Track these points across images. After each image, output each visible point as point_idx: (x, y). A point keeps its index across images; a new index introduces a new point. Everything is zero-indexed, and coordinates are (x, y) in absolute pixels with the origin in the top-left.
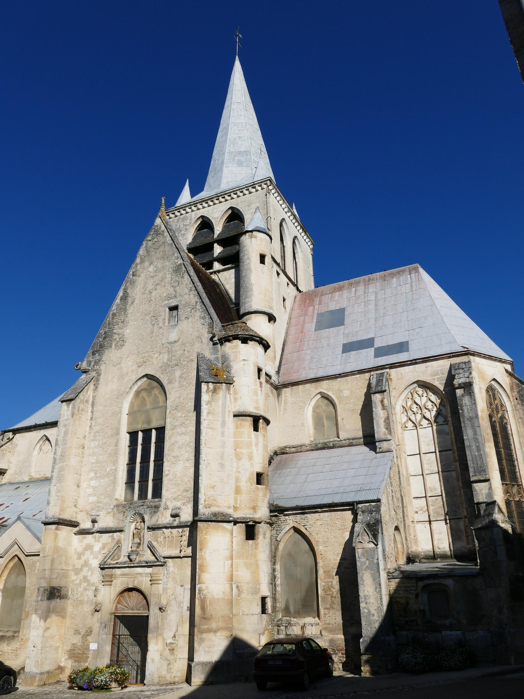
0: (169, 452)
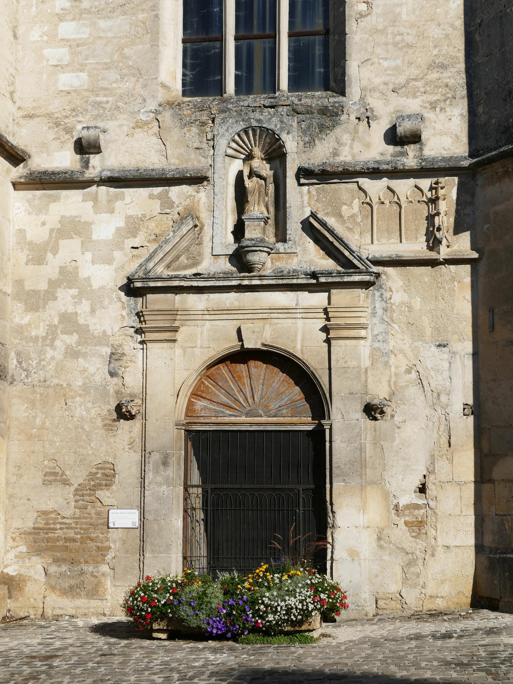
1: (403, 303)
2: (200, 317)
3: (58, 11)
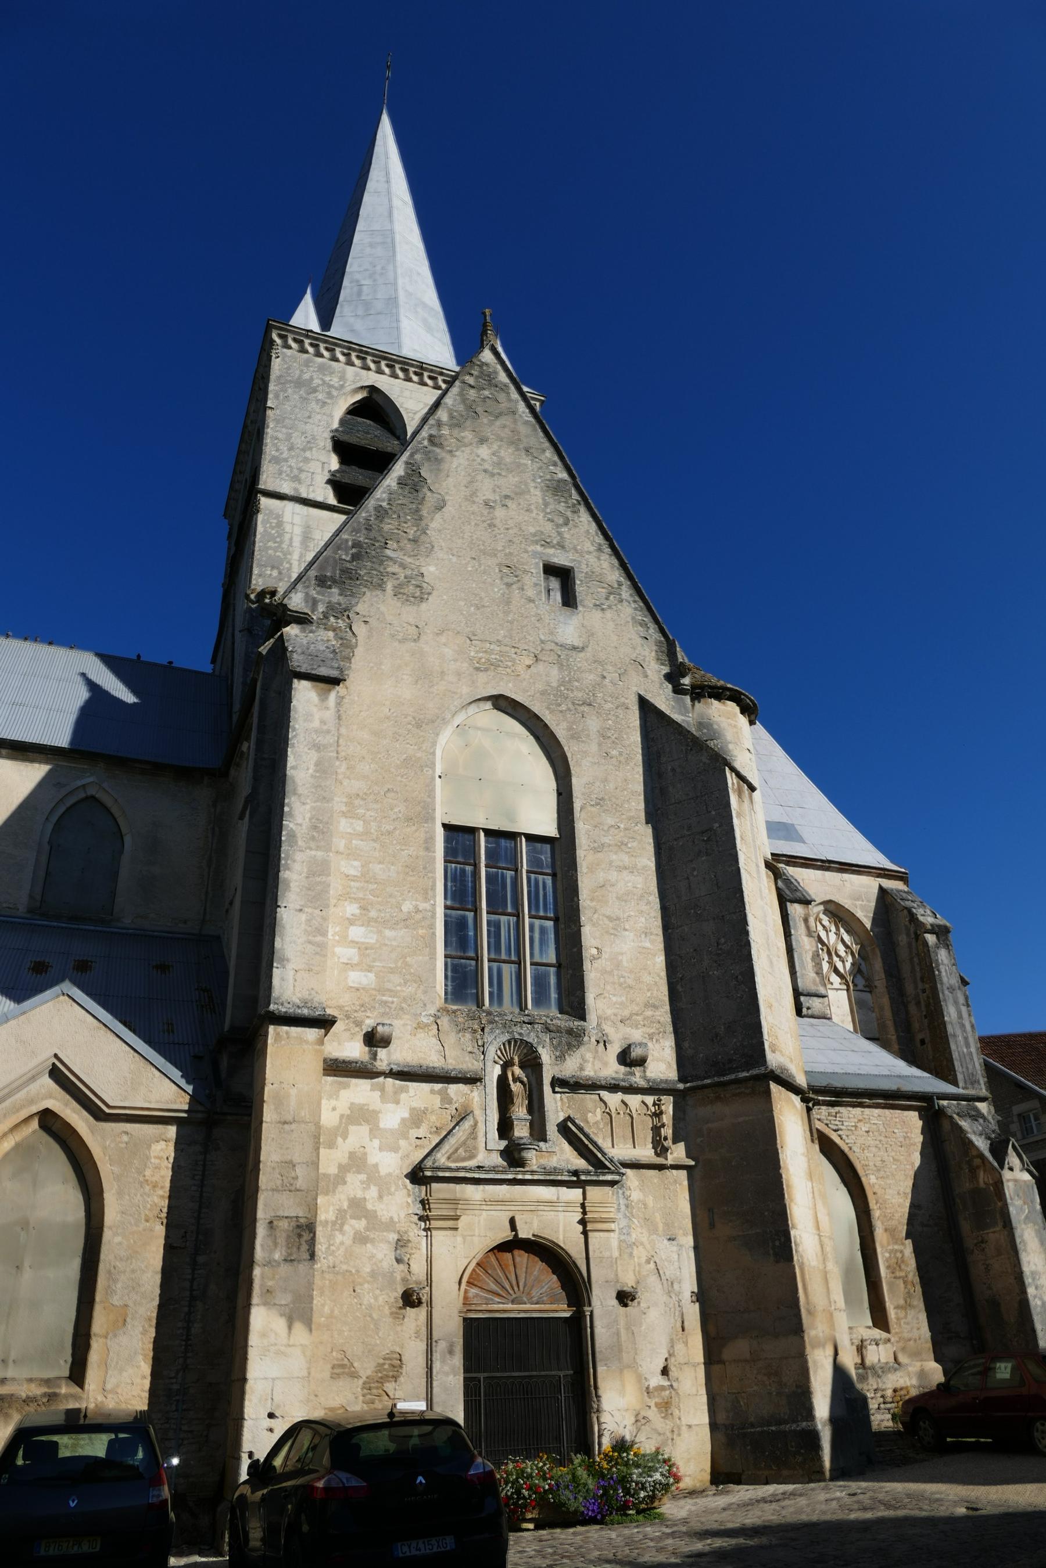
0: (594, 903)
1: (639, 1201)
2: (478, 1207)
3: (348, 915)
